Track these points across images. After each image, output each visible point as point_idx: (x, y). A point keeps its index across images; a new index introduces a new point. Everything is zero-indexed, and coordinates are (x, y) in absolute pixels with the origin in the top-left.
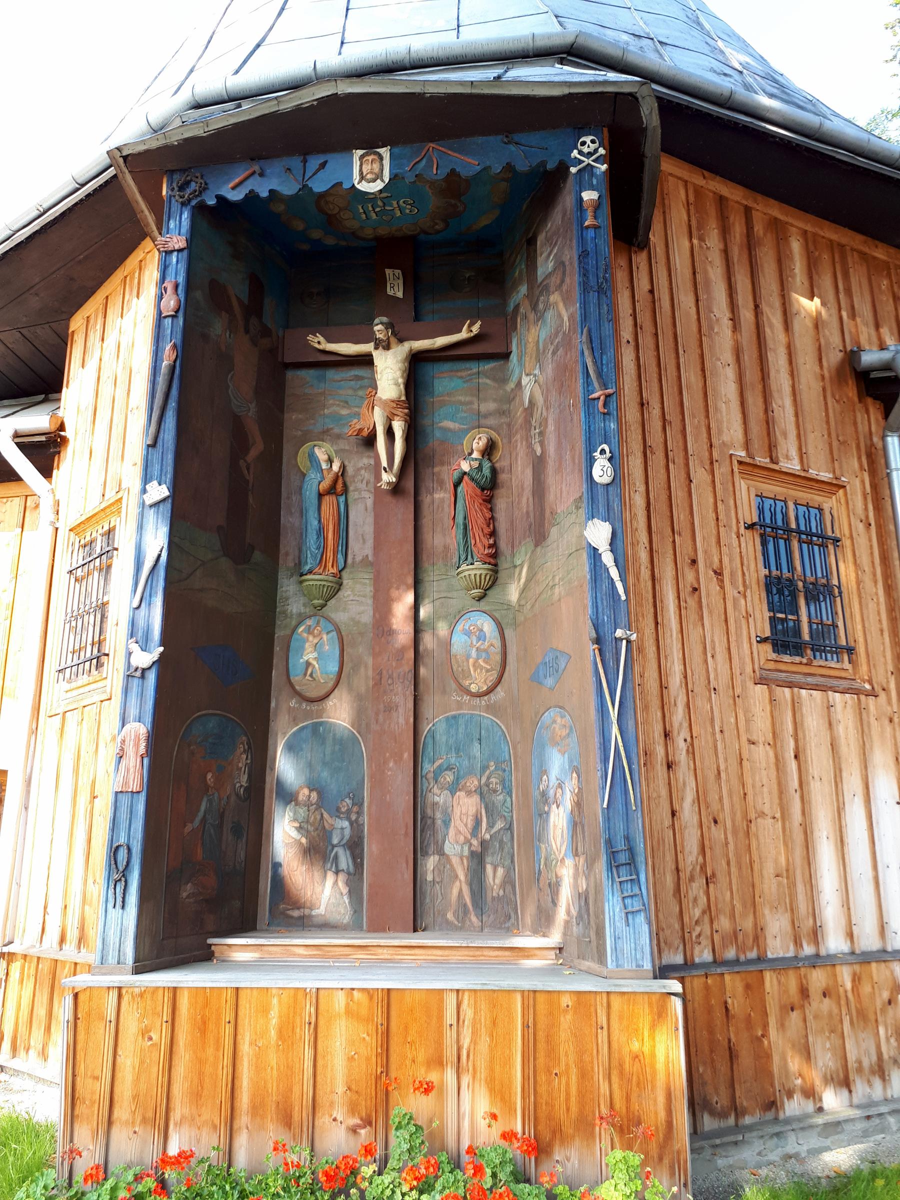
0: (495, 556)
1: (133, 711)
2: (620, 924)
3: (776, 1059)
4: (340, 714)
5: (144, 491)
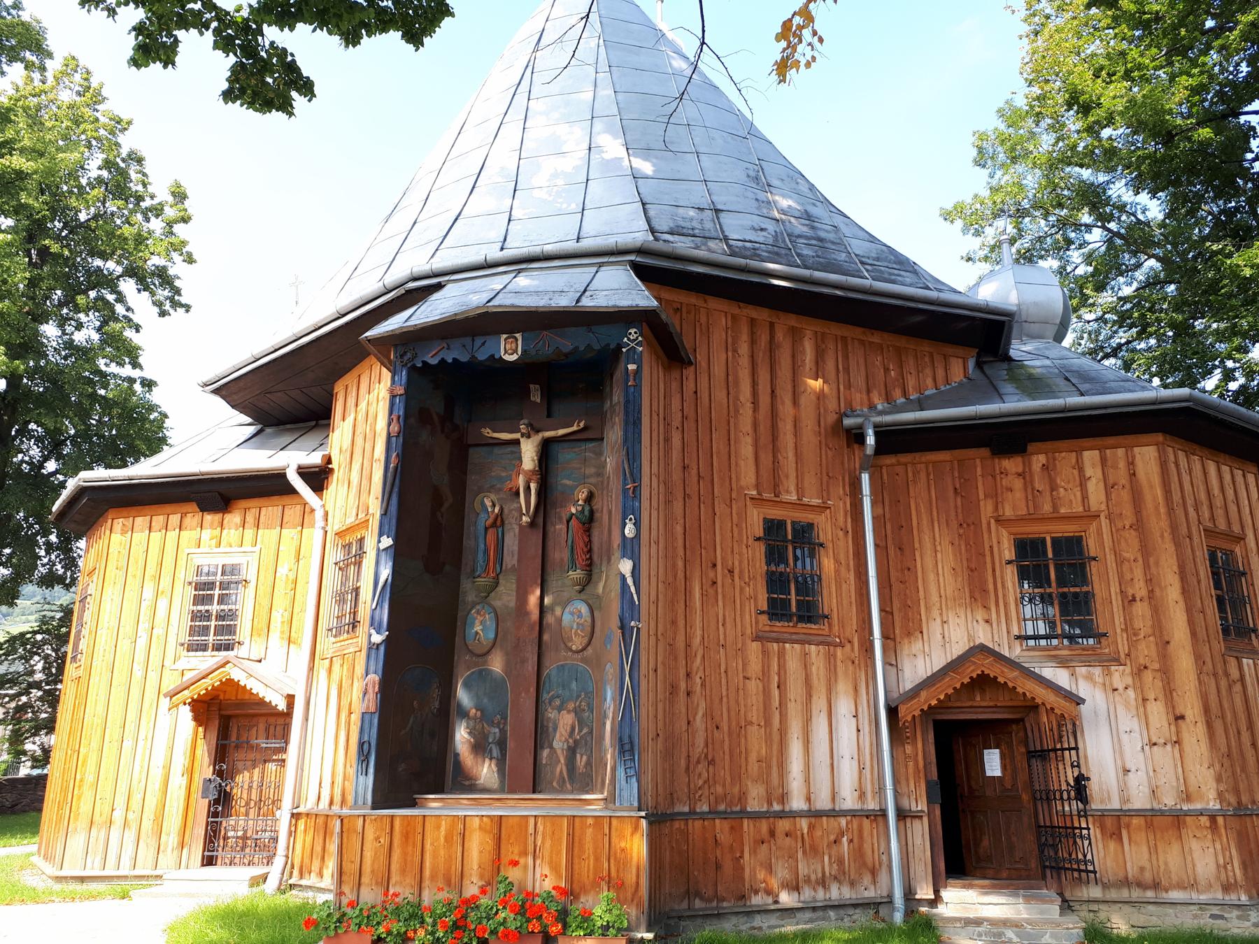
0: (590, 565)
1: (372, 668)
2: (623, 782)
3: (747, 871)
4: (496, 665)
5: (379, 541)
